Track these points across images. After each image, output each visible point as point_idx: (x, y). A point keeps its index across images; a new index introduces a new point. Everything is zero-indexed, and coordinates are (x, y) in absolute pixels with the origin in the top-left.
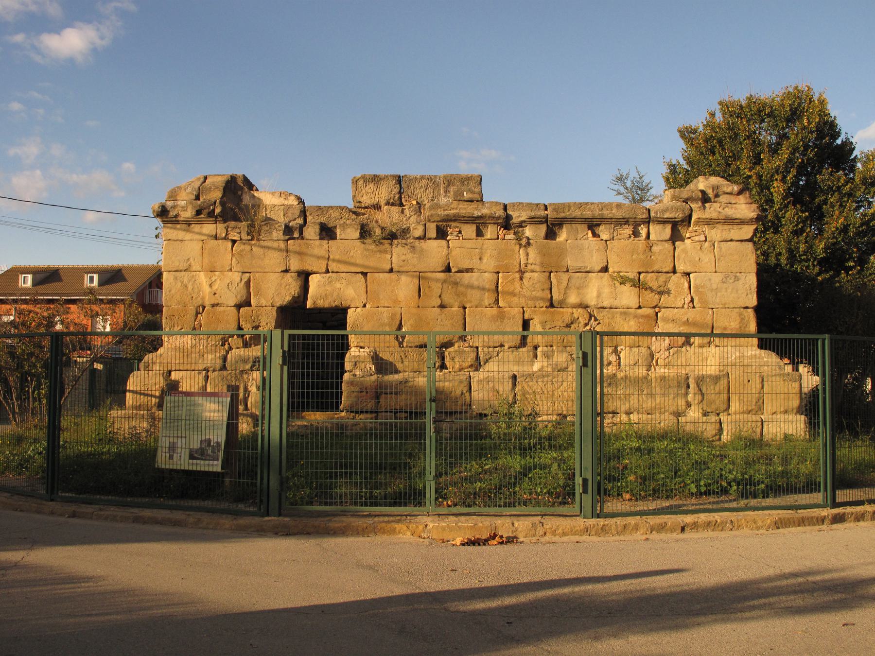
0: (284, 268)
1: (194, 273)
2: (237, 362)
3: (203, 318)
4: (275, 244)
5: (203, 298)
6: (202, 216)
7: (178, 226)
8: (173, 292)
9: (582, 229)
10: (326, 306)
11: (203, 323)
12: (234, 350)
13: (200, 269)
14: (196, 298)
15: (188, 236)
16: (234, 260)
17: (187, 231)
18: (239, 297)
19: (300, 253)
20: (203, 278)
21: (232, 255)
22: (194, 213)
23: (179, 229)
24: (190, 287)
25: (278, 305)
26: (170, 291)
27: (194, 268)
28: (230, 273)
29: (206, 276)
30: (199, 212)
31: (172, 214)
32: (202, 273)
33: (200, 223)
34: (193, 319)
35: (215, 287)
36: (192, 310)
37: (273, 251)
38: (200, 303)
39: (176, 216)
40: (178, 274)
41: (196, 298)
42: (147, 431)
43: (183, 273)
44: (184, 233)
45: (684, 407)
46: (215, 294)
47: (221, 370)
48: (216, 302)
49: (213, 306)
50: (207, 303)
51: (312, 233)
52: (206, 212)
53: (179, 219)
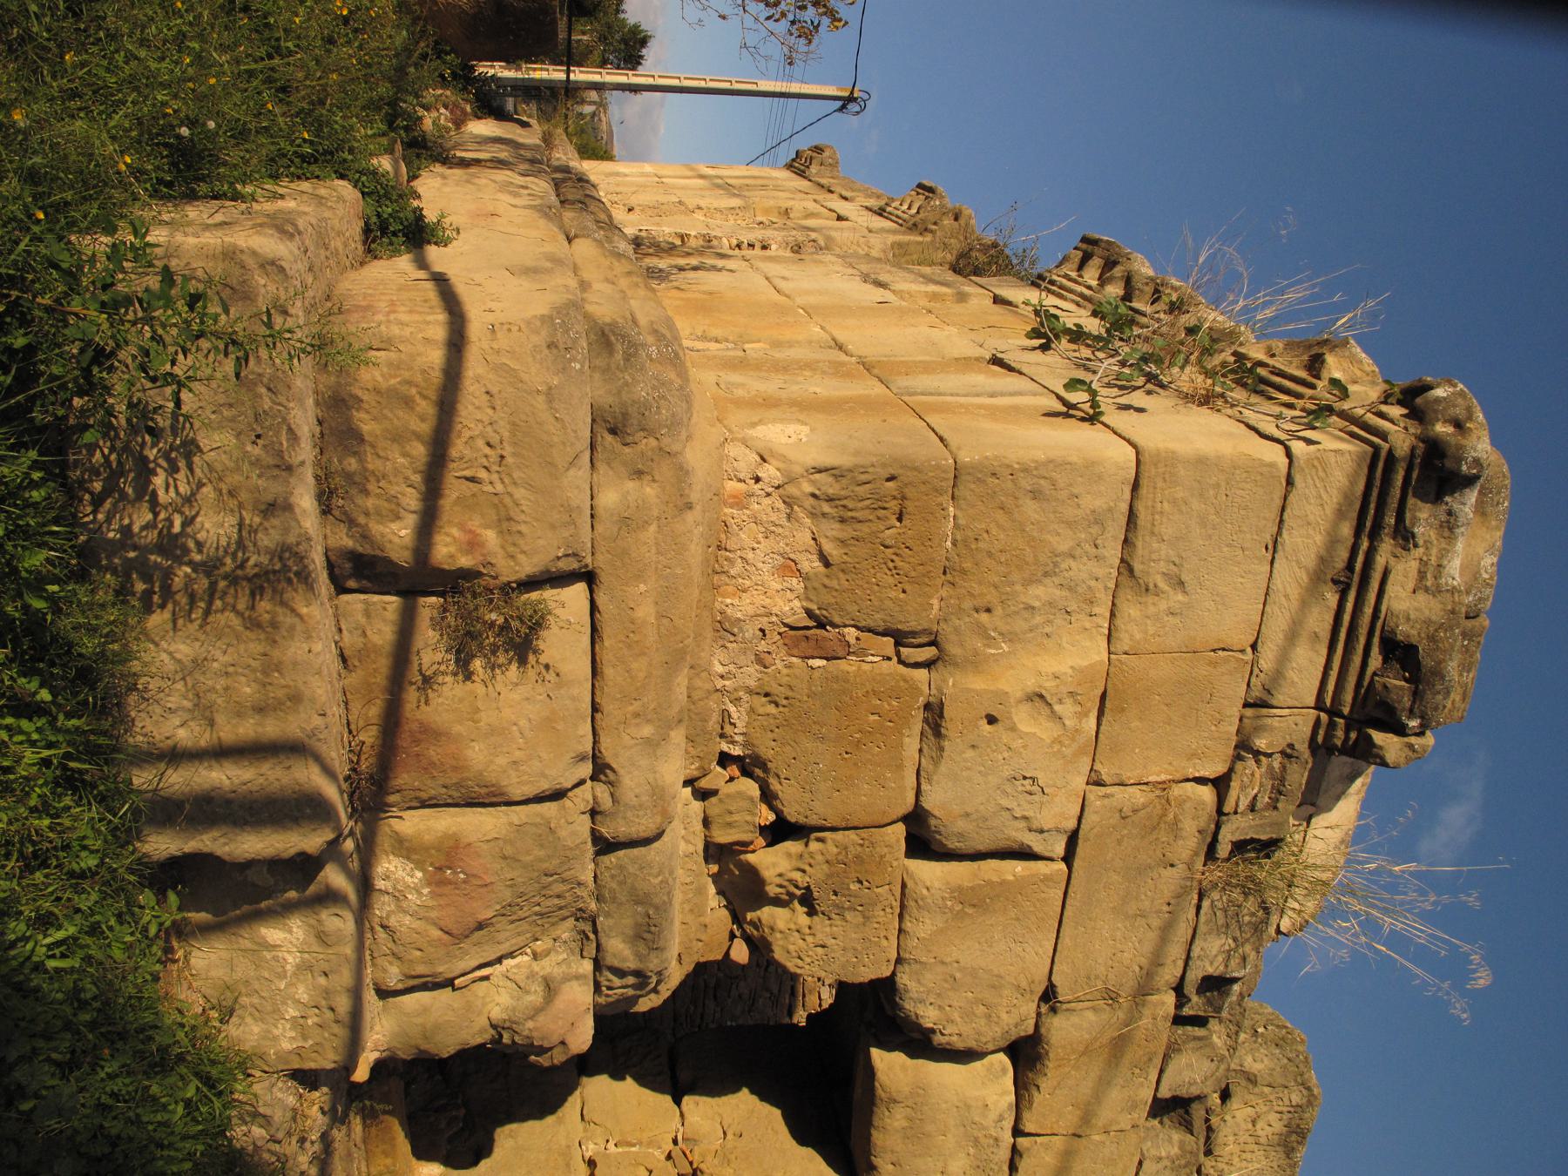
0: (1063, 993)
1: (1103, 610)
2: (641, 899)
3: (876, 663)
4: (1176, 952)
5: (975, 663)
6: (1376, 661)
7: (1347, 530)
8: (1030, 508)
9: (900, 968)
10: (877, 1137)
11: (848, 666)
12: (697, 806)
13: (1123, 642)
14: (982, 631)
15: (1291, 577)
16: (1137, 796)
17: (1317, 578)
18: (961, 825)
19: (1119, 1045)
20: (1077, 653)
21: (1164, 786)
22: (1404, 630)
23: (1335, 525)
24: (1039, 593)
25: (903, 979)
26: (1035, 494)
27: (1130, 610)
28: (1079, 782)
29: (1083, 674)
30: (1400, 653)
31: (1423, 517)
32: (1097, 652)
33: (1342, 636)
34: (878, 620)
35: (1026, 720)
36: (927, 608)
37: (1148, 947)
38: (953, 649)
39: (1405, 536)
40: (1117, 529)
41: (982, 631)
42: (171, 546)
43: (1113, 552)
44: (1310, 560)
45: (335, 1132)
46: (992, 720)
47: (597, 838)
48: (950, 727)
49: (934, 715)
50: (953, 685)
51: (1187, 1076)
52: (1397, 683)
53: (1386, 548)
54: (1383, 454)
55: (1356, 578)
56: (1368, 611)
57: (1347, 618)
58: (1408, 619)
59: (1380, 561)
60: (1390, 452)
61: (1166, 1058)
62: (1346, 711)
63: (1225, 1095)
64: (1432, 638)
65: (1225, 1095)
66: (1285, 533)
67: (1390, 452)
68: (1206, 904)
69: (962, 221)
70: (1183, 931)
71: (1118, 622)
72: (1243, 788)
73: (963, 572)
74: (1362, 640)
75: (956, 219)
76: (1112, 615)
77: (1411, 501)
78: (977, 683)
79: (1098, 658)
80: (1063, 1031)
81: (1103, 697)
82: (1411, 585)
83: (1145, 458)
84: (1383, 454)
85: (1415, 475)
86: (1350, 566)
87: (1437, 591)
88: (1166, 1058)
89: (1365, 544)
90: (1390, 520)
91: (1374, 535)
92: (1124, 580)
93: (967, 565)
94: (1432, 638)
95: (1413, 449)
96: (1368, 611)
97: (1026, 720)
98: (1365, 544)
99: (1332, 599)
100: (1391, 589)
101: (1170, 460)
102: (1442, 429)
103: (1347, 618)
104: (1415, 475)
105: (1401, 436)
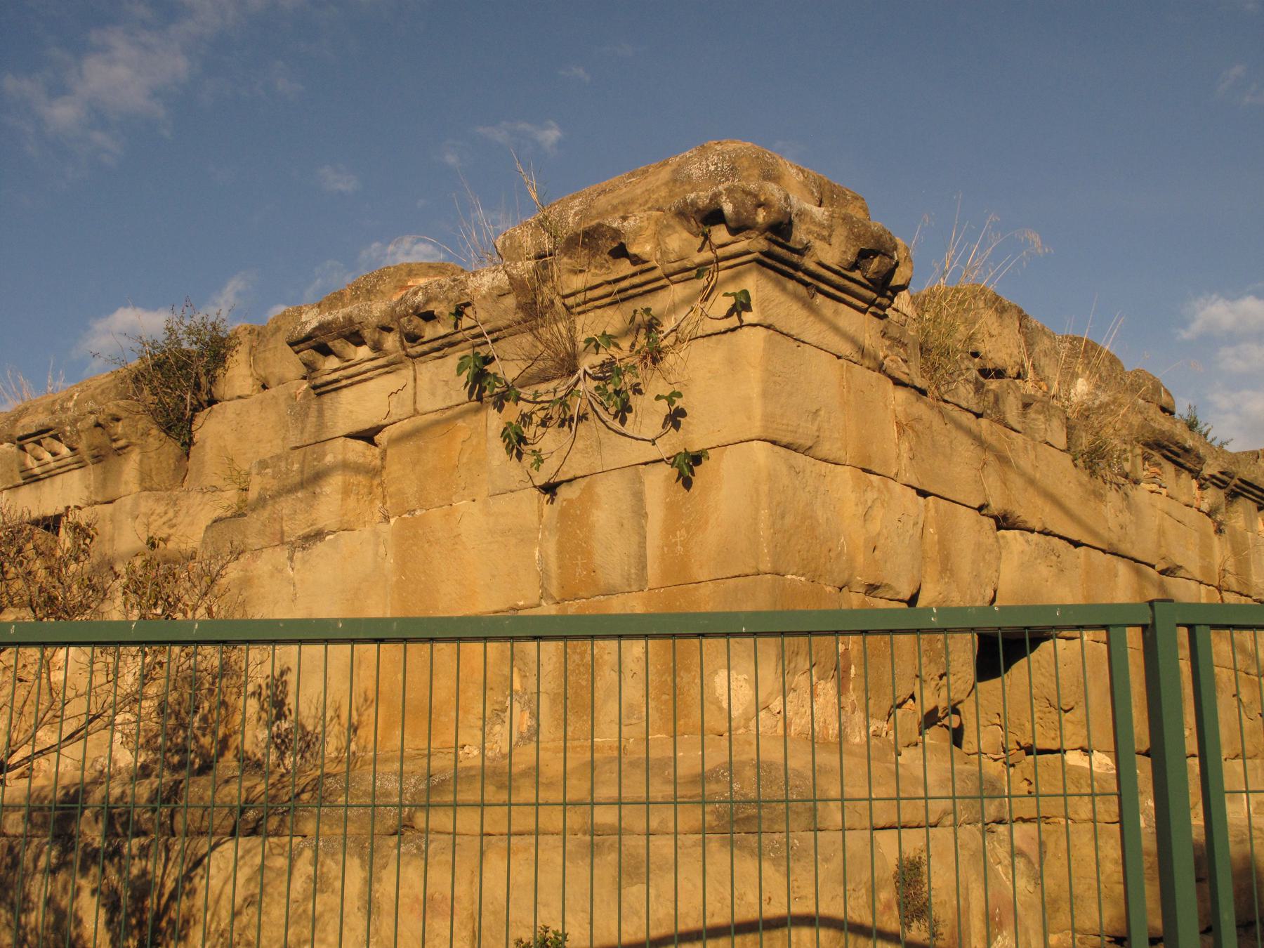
6: (857, 275)
7: (791, 285)
8: (789, 520)
22: (851, 257)
52: (874, 264)
54: (761, 257)
55: (815, 282)
56: (834, 277)
57: (832, 290)
58: (845, 252)
59: (812, 267)
60: (761, 253)
61: (1007, 426)
62: (875, 296)
63: (975, 355)
64: (858, 237)
65: (975, 355)
66: (792, 333)
67: (761, 253)
68: (946, 397)
69: (124, 414)
70: (956, 413)
71: (831, 458)
72: (898, 368)
73: (816, 570)
74: (846, 283)
75: (118, 420)
76: (825, 461)
77: (791, 244)
78: (860, 559)
79: (848, 474)
80: (996, 506)
81: (864, 470)
82: (827, 246)
83: (764, 436)
84: (761, 257)
85: (780, 240)
86: (806, 285)
87: (831, 228)
88: (1007, 426)
89: (800, 274)
90: (795, 258)
91: (796, 267)
92: (811, 452)
93: (813, 565)
94: (858, 237)
95: (766, 238)
96: (834, 277)
97: (875, 527)
98: (800, 274)
99: (820, 299)
100: (828, 262)
101: (768, 418)
102: (761, 216)
103: (832, 290)
104: (780, 240)
105: (753, 243)
